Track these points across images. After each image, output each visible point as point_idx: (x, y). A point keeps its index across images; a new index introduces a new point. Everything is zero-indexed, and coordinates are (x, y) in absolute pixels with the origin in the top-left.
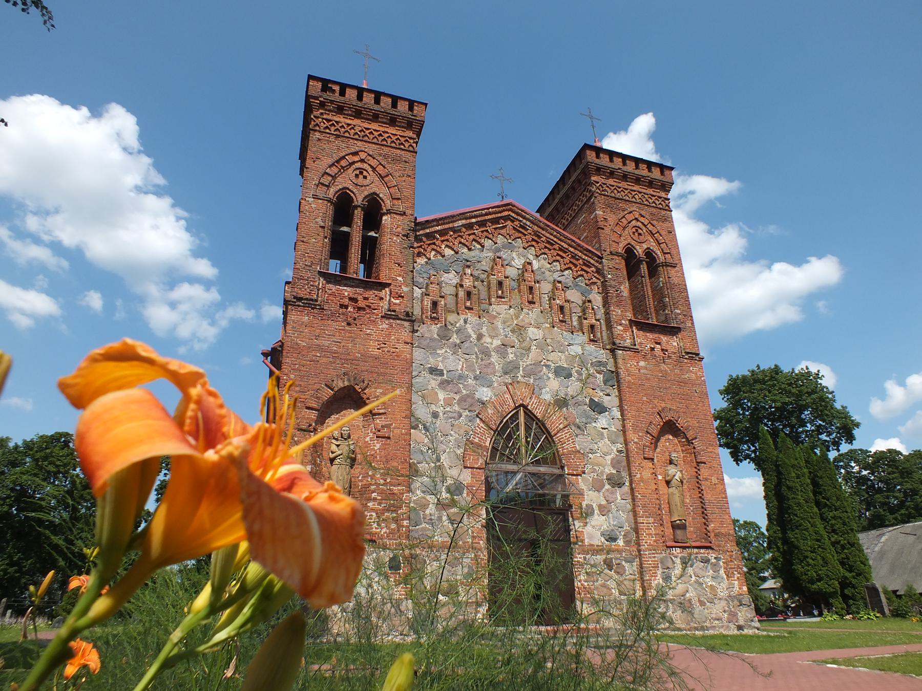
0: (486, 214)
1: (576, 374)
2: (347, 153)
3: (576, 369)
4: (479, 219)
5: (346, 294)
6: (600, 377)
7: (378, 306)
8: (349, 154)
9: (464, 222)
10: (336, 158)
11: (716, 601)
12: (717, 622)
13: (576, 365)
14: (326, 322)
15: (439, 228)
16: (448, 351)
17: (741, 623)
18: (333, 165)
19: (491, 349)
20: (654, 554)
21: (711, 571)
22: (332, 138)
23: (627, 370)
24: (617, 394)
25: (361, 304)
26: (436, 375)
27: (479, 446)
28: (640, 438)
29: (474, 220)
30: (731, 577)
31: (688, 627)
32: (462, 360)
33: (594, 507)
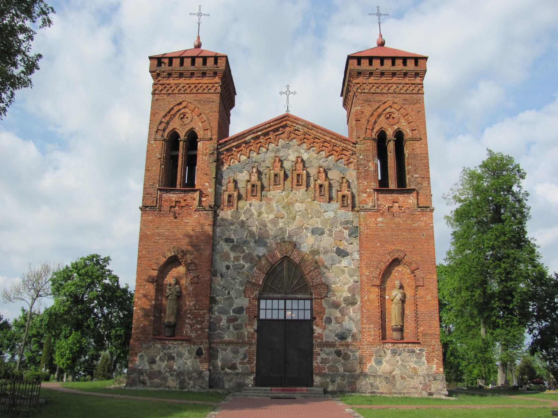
0: (269, 127)
1: (328, 232)
2: (174, 105)
3: (328, 228)
4: (264, 131)
5: (174, 199)
6: (346, 232)
7: (192, 204)
8: (176, 105)
9: (253, 136)
10: (168, 110)
11: (415, 377)
12: (413, 390)
13: (328, 226)
14: (162, 218)
15: (235, 144)
16: (238, 226)
17: (433, 390)
18: (166, 115)
19: (267, 222)
20: (370, 347)
21: (415, 358)
22: (165, 97)
23: (366, 225)
24: (358, 242)
25: (183, 204)
26: (230, 242)
27: (254, 284)
28: (371, 272)
29: (260, 133)
30: (431, 362)
31: (389, 392)
32: (246, 231)
33: (332, 318)
